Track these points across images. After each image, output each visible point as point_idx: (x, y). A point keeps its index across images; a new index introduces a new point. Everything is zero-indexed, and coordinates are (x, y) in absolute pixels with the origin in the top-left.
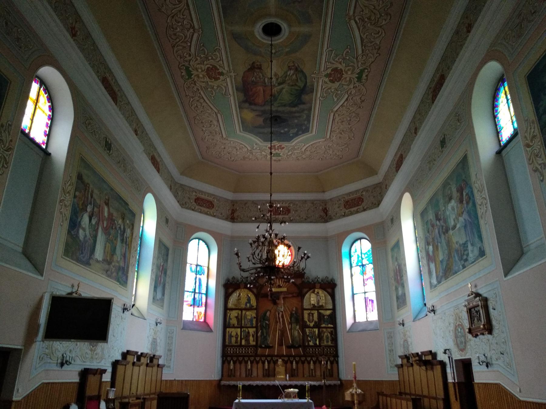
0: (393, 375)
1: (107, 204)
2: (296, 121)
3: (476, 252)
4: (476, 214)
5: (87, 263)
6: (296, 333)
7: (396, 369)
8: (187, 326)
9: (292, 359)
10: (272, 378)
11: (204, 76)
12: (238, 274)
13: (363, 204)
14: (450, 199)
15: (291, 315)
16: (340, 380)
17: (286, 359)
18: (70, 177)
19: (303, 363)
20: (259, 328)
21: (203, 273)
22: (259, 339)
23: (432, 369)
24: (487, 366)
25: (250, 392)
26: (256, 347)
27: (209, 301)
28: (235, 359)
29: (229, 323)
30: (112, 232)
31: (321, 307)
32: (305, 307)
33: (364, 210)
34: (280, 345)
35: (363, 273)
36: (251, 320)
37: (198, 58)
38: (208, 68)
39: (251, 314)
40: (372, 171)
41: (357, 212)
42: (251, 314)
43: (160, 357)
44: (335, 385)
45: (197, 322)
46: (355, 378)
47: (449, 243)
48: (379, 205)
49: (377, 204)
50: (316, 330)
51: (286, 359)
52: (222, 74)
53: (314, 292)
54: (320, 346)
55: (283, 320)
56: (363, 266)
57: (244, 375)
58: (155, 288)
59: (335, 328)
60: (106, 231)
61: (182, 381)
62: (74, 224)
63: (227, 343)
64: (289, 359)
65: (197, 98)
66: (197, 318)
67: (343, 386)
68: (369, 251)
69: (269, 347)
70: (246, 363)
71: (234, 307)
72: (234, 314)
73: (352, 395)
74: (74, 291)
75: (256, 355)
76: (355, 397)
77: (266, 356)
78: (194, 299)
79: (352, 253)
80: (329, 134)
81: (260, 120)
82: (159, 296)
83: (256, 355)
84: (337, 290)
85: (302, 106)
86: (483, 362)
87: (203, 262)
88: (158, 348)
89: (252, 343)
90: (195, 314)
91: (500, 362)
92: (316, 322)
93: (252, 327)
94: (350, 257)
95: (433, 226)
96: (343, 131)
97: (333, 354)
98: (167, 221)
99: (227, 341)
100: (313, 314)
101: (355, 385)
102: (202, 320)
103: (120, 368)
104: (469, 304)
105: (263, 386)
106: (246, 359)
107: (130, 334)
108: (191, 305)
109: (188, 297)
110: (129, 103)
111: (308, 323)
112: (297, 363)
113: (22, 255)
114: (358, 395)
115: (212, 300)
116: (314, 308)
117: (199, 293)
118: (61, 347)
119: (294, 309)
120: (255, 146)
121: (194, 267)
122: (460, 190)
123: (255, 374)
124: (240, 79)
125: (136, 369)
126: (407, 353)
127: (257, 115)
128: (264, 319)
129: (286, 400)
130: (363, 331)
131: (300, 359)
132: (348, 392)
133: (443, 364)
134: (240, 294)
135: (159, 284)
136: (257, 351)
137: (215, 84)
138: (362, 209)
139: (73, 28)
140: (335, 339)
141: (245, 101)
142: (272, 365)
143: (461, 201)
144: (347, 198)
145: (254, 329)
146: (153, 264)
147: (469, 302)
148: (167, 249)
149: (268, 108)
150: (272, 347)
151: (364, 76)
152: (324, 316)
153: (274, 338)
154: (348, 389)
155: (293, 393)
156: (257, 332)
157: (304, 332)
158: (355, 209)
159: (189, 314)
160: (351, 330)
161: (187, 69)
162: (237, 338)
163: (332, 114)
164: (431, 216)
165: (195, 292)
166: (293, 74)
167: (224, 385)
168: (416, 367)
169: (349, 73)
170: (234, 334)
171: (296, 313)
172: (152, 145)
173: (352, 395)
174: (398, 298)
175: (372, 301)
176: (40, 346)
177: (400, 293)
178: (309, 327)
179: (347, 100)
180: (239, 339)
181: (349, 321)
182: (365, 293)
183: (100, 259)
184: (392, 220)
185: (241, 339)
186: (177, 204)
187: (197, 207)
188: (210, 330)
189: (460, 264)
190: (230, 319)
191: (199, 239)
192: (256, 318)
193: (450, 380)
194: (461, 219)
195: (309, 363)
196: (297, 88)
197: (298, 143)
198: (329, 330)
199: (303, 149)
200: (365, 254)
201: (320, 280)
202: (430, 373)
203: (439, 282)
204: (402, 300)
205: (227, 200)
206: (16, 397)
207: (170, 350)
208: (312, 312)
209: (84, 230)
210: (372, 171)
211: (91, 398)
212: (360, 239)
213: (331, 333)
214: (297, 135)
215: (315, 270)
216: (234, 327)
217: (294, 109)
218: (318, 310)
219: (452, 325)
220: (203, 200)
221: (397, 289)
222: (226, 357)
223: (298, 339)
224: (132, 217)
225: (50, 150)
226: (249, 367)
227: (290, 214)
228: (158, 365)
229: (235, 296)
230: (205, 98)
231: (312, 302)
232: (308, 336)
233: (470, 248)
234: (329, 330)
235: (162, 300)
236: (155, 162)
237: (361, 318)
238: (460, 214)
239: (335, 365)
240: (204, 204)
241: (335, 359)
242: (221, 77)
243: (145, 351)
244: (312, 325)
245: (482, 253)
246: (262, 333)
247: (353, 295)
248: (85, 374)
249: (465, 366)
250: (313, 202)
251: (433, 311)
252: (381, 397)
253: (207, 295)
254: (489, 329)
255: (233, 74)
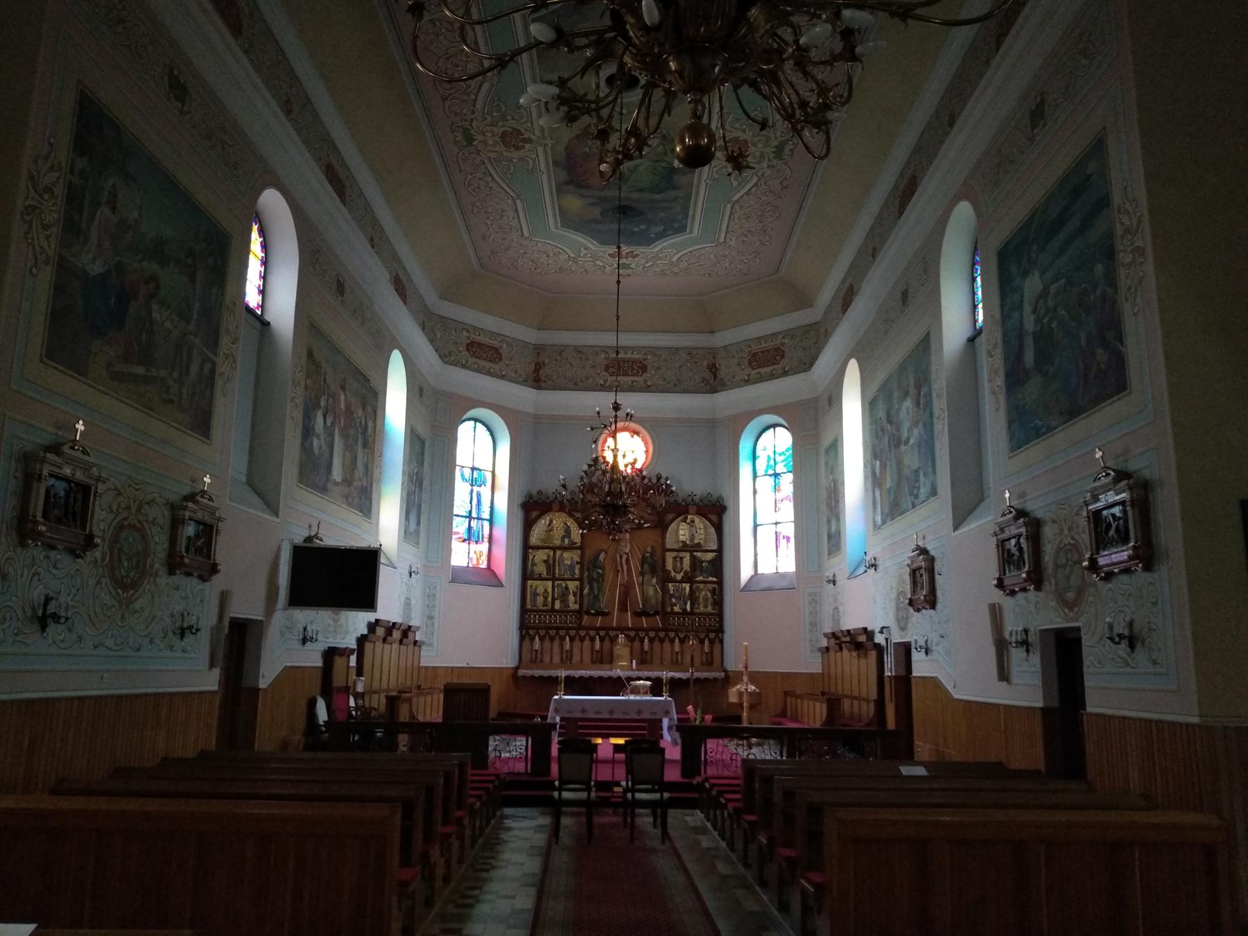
0: (814, 665)
1: (343, 388)
2: (662, 214)
3: (929, 490)
4: (932, 430)
5: (323, 490)
6: (651, 592)
7: (819, 654)
8: (460, 576)
9: (642, 634)
10: (608, 666)
11: (496, 143)
12: (550, 484)
13: (785, 362)
14: (906, 394)
15: (643, 561)
16: (725, 671)
17: (632, 634)
18: (51, 145)
19: (662, 641)
20: (586, 581)
21: (484, 483)
22: (586, 602)
23: (866, 656)
24: (1132, 646)
25: (575, 685)
26: (579, 612)
27: (495, 532)
28: (542, 632)
29: (532, 571)
30: (351, 432)
31: (698, 548)
32: (668, 546)
33: (785, 373)
34: (623, 609)
35: (776, 488)
36: (571, 567)
37: (489, 118)
38: (504, 133)
39: (570, 557)
40: (805, 302)
41: (772, 377)
42: (570, 557)
43: (418, 628)
44: (715, 679)
45: (476, 569)
46: (746, 668)
47: (899, 463)
48: (812, 364)
49: (807, 364)
50: (687, 586)
51: (632, 634)
52: (529, 141)
53: (684, 520)
54: (692, 613)
55: (629, 569)
56: (776, 475)
57: (557, 660)
58: (408, 513)
59: (720, 583)
60: (345, 436)
61: (453, 668)
62: (308, 432)
63: (529, 607)
64: (637, 634)
65: (479, 175)
66: (475, 562)
67: (729, 679)
68: (787, 450)
69: (604, 614)
70: (562, 639)
71: (539, 543)
72: (541, 555)
73: (740, 694)
74: (313, 534)
75: (580, 627)
76: (745, 698)
77: (597, 629)
78: (470, 528)
79: (758, 453)
80: (723, 235)
81: (596, 211)
82: (413, 527)
83: (580, 627)
84: (727, 518)
85: (673, 193)
86: (1120, 636)
87: (484, 463)
88: (413, 615)
89: (573, 606)
90: (472, 555)
91: (939, 648)
92: (686, 573)
93: (573, 579)
94: (754, 458)
95: (883, 430)
96: (749, 232)
97: (715, 629)
98: (421, 391)
99: (528, 602)
100: (682, 559)
101: (745, 678)
102: (484, 565)
103: (368, 646)
104: (1002, 530)
105: (591, 678)
106: (562, 633)
107: (394, 598)
108: (464, 541)
109: (460, 526)
110: (361, 195)
111: (673, 574)
112: (651, 641)
113: (248, 488)
114: (751, 694)
115: (501, 531)
116: (684, 547)
117: (479, 518)
118: (303, 616)
119: (649, 549)
120: (584, 252)
121: (467, 473)
122: (918, 387)
123: (576, 658)
124: (561, 148)
125: (387, 647)
126: (836, 630)
127: (590, 204)
128: (595, 567)
129: (632, 697)
130: (769, 589)
131: (657, 635)
132: (734, 689)
133: (879, 649)
134: (551, 521)
135: (412, 507)
136: (581, 619)
137: (516, 155)
138: (781, 371)
139: (288, 102)
140: (719, 603)
141: (567, 183)
142: (607, 644)
143: (918, 404)
144: (755, 347)
145: (577, 583)
146: (404, 472)
147: (913, 560)
148: (423, 443)
149: (613, 193)
150: (608, 614)
151: (787, 151)
152: (702, 562)
153: (610, 597)
154: (736, 684)
155: (644, 686)
156: (582, 589)
157: (665, 590)
158: (768, 369)
159: (461, 555)
160: (747, 588)
161: (466, 131)
162: (546, 598)
163: (729, 206)
164: (881, 414)
165: (470, 517)
166: (658, 145)
167: (524, 677)
168: (845, 652)
169: (760, 145)
170: (540, 590)
171: (652, 556)
172: (395, 258)
173: (740, 694)
174: (829, 536)
175: (788, 539)
176: (280, 617)
177: (834, 528)
178: (674, 581)
179: (756, 185)
180: (550, 599)
181: (746, 573)
182: (776, 524)
183: (339, 480)
184: (830, 400)
185: (554, 599)
186: (437, 357)
187: (472, 360)
188: (499, 584)
189: (910, 499)
190: (534, 564)
191: (476, 420)
192: (581, 563)
193: (887, 673)
194: (916, 431)
195: (672, 641)
196: (664, 165)
197: (666, 248)
198: (710, 586)
199: (675, 259)
200: (780, 454)
201: (697, 499)
202: (863, 661)
203: (884, 522)
204: (835, 541)
205: (526, 345)
206: (263, 684)
207: (431, 617)
208: (682, 554)
209: (319, 438)
210: (805, 302)
211: (340, 690)
212: (774, 426)
213: (713, 592)
214: (661, 236)
215: (689, 482)
216: (541, 578)
217: (658, 197)
218: (691, 552)
219: (894, 591)
220: (480, 345)
221: (829, 521)
222: (526, 629)
223: (653, 601)
224: (374, 399)
225: (268, 318)
226: (568, 647)
227: (645, 375)
228: (415, 642)
229: (543, 523)
230: (495, 175)
231: (682, 538)
232: (672, 596)
233: (922, 479)
234: (710, 586)
235: (417, 532)
236: (400, 287)
237: (766, 568)
238: (915, 424)
239: (717, 645)
240: (482, 353)
241: (717, 636)
242: (527, 146)
243: (398, 620)
244: (679, 577)
245: (934, 492)
246: (591, 589)
247: (756, 526)
248: (331, 654)
249: (905, 650)
250: (690, 352)
251: (874, 566)
252: (789, 699)
253: (491, 521)
254: (932, 602)
255: (549, 142)
